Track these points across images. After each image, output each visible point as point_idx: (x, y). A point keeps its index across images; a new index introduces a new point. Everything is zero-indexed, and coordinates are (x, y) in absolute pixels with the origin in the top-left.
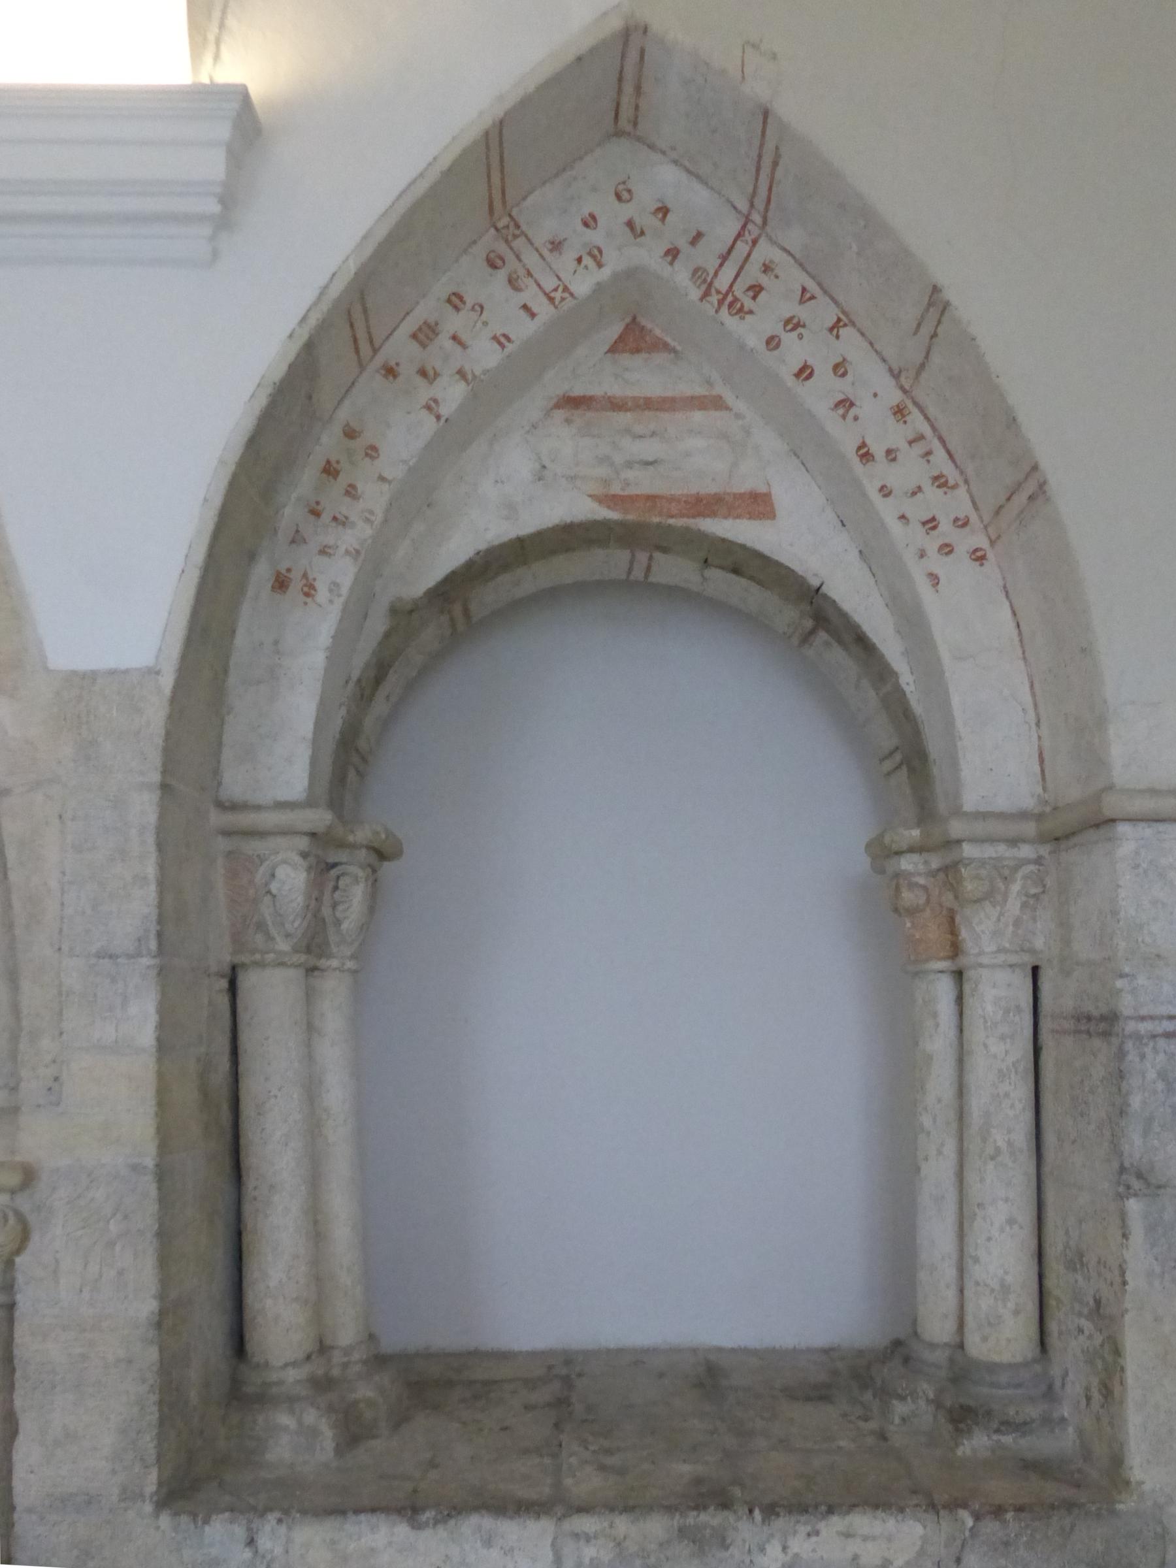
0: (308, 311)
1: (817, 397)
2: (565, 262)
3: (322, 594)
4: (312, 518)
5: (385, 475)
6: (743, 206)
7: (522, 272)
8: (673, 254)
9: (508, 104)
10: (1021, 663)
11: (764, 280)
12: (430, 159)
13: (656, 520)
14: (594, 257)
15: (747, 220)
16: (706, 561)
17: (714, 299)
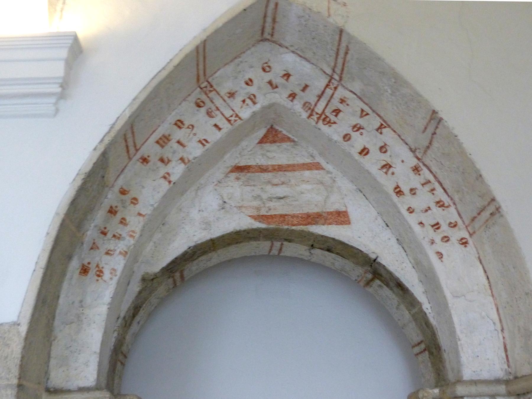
0: (104, 136)
1: (372, 164)
2: (236, 103)
3: (107, 275)
4: (102, 236)
5: (142, 212)
6: (329, 71)
7: (214, 108)
8: (293, 96)
9: (208, 33)
10: (491, 298)
11: (341, 107)
12: (168, 61)
13: (286, 227)
14: (251, 99)
15: (332, 78)
16: (312, 246)
17: (315, 117)
